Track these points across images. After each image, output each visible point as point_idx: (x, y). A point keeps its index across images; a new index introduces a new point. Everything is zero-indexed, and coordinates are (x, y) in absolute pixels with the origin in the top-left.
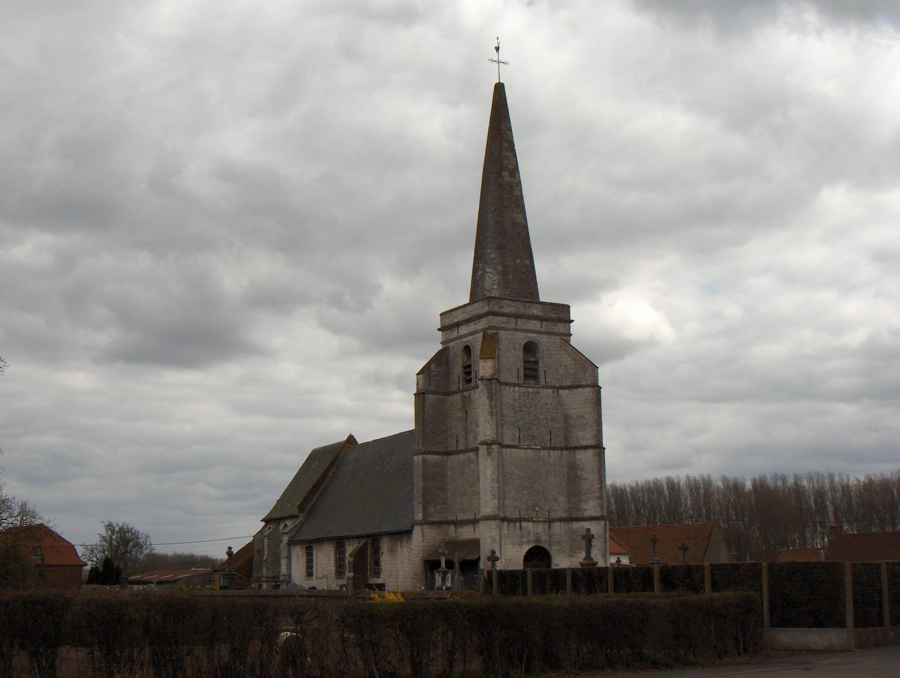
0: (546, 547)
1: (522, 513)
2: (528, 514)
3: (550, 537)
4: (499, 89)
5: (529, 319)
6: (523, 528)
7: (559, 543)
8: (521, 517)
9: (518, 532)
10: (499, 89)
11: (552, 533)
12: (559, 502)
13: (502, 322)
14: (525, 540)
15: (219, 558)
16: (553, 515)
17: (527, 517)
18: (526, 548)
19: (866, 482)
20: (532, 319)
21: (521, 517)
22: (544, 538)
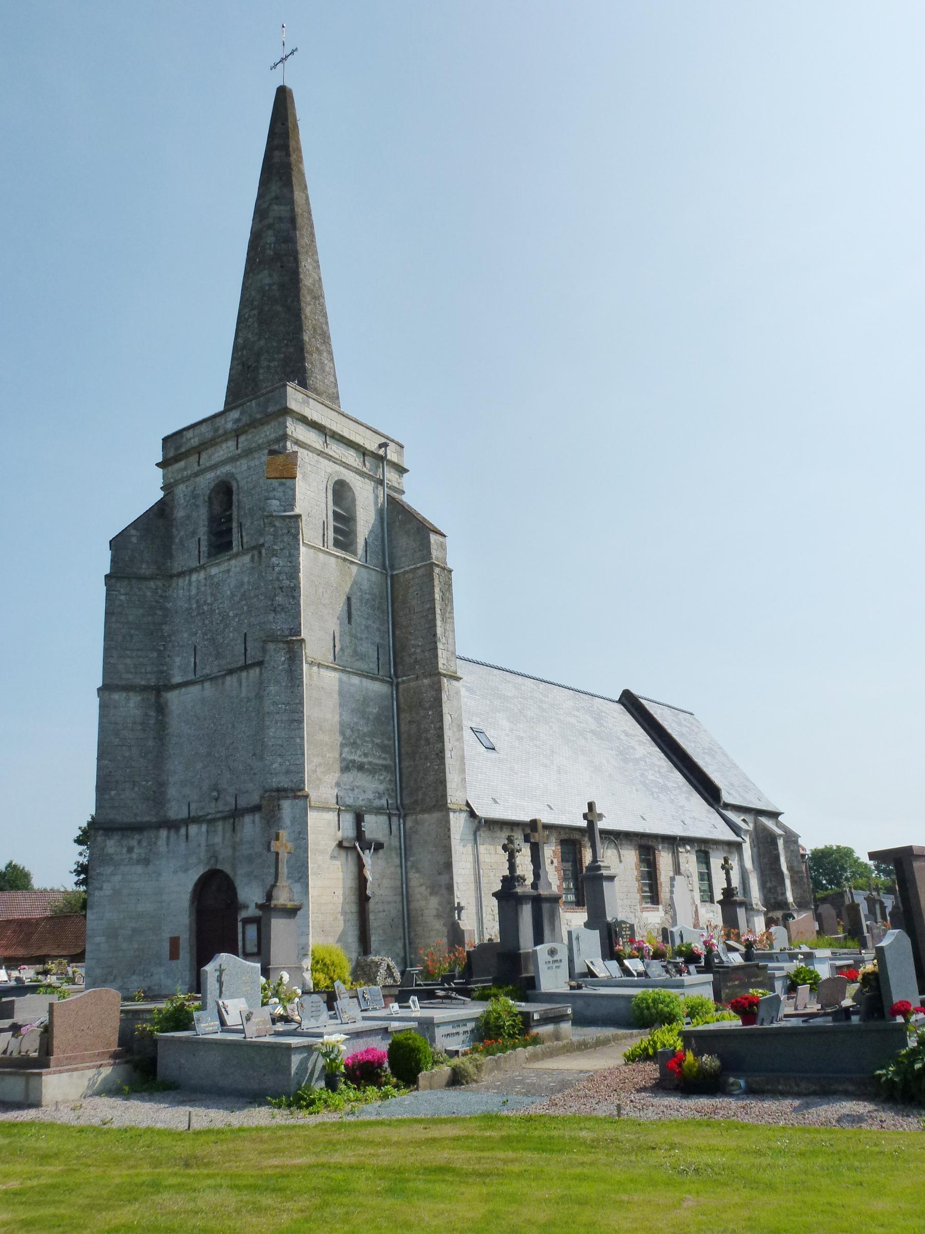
0: (227, 869)
1: (193, 806)
2: (203, 808)
3: (234, 849)
4: (283, 98)
5: (216, 444)
6: (190, 839)
7: (250, 859)
8: (192, 814)
9: (183, 845)
10: (283, 98)
11: (238, 840)
12: (254, 774)
13: (185, 469)
14: (193, 860)
15: (57, 886)
16: (243, 803)
17: (200, 814)
18: (193, 876)
19: (347, 718)
20: (222, 442)
21: (192, 814)
22: (225, 853)
